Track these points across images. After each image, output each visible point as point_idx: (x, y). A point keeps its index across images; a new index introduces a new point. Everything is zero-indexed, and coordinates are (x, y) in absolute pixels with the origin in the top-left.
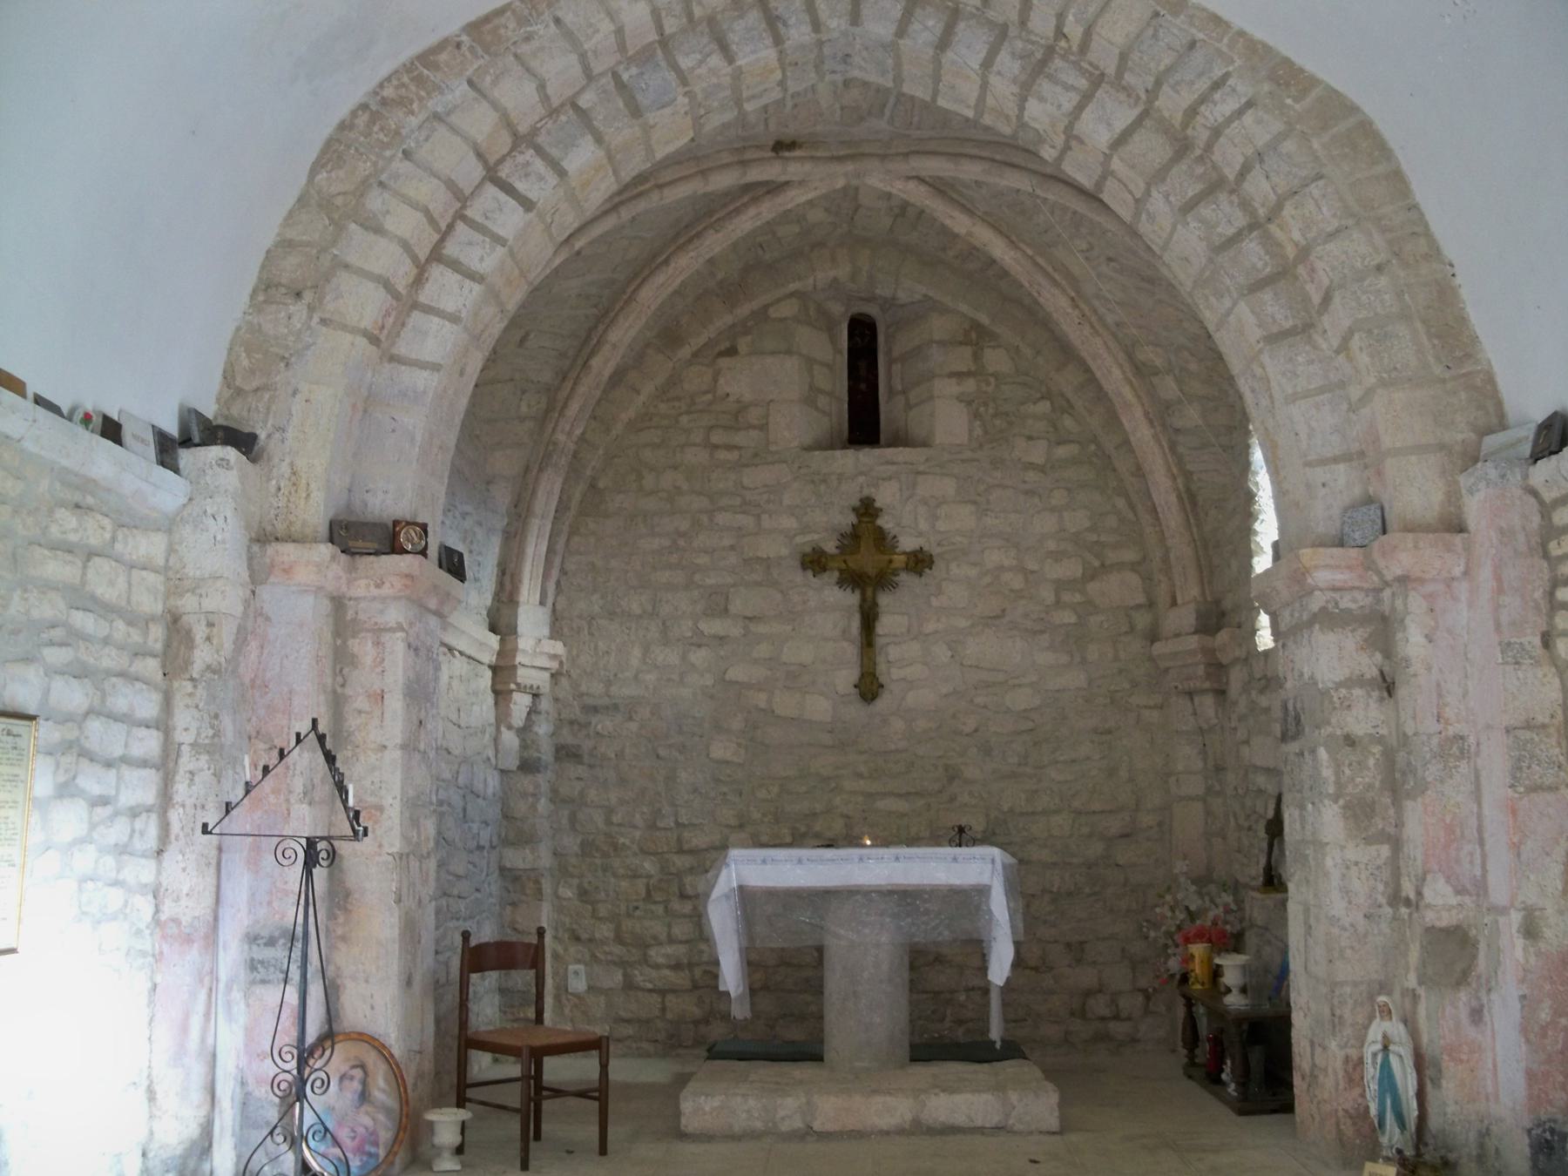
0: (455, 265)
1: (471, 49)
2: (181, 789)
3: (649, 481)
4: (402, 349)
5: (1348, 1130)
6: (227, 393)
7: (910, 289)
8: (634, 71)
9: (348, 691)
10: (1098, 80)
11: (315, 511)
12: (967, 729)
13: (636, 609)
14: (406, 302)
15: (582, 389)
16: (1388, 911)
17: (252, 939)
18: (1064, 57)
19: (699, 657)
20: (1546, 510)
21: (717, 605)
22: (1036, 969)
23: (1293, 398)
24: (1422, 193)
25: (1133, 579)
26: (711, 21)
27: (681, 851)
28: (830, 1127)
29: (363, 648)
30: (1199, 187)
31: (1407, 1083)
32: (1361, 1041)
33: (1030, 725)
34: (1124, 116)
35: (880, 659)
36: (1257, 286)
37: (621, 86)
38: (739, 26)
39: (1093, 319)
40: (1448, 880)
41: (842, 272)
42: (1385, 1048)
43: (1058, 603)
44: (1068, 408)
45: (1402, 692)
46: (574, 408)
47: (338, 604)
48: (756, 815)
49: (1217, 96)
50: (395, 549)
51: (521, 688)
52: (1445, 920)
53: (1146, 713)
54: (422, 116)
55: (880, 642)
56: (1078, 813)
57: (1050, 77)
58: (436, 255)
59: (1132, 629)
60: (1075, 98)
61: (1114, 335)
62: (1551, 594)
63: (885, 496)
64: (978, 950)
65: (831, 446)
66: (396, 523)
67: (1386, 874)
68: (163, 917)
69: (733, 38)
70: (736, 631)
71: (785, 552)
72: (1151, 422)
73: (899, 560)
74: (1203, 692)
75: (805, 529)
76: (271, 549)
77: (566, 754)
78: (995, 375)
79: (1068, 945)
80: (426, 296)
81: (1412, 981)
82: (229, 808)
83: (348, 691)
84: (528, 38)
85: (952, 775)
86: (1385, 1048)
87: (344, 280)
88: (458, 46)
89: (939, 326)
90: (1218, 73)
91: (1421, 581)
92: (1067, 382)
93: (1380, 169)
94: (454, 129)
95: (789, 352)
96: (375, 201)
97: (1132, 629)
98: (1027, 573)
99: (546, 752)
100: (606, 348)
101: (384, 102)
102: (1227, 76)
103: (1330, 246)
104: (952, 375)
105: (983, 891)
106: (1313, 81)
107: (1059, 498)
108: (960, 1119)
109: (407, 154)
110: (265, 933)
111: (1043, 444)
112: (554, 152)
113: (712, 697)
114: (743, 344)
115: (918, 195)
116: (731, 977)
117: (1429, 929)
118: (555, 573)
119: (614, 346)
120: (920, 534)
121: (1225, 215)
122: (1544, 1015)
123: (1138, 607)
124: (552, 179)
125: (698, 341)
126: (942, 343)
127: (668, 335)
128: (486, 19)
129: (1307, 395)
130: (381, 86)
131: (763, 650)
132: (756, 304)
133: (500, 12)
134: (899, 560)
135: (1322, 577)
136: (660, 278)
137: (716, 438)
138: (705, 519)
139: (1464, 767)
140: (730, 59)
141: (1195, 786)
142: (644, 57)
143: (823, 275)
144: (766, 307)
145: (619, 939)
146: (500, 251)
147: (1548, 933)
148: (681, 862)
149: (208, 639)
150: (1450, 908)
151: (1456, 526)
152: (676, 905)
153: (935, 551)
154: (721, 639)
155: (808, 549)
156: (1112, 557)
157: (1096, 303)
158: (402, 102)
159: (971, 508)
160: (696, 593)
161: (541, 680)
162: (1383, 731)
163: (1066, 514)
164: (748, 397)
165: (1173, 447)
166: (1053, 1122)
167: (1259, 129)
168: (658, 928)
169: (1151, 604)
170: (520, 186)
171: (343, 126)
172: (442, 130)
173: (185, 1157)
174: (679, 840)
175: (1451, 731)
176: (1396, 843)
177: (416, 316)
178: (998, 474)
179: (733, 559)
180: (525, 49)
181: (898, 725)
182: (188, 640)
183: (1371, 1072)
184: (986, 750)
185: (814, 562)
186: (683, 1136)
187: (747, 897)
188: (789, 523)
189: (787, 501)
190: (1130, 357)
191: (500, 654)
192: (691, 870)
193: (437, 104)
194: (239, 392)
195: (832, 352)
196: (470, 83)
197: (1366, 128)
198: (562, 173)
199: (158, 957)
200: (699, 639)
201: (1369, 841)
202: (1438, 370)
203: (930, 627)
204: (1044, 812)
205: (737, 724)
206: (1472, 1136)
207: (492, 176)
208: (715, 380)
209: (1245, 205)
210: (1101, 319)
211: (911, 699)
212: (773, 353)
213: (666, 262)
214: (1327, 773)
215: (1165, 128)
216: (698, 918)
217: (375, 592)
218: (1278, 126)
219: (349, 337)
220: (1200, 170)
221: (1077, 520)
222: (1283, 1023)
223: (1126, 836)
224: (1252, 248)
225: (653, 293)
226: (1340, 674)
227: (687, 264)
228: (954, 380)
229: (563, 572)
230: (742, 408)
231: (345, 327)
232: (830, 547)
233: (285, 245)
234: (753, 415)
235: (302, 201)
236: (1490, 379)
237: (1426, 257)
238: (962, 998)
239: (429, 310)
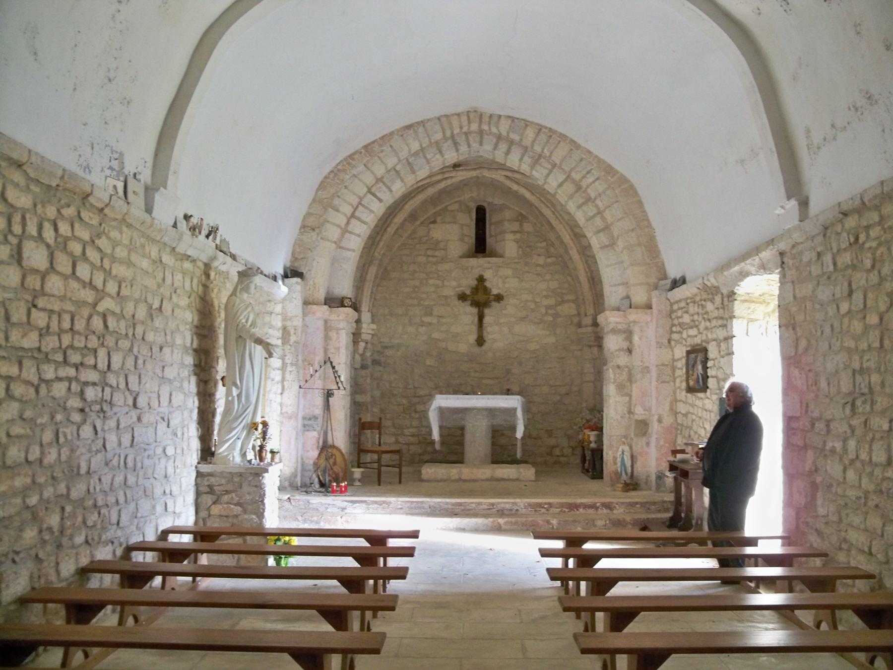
0: (359, 219)
1: (365, 154)
2: (287, 376)
3: (405, 268)
4: (343, 244)
5: (613, 475)
6: (293, 259)
7: (498, 201)
8: (413, 158)
9: (329, 347)
10: (554, 166)
11: (321, 295)
12: (514, 356)
13: (400, 313)
14: (345, 231)
15: (384, 238)
16: (627, 416)
17: (304, 418)
18: (544, 158)
19: (422, 330)
20: (672, 305)
21: (429, 312)
22: (535, 438)
23: (607, 266)
24: (647, 207)
25: (573, 306)
26: (437, 142)
27: (415, 396)
28: (467, 478)
29: (333, 334)
30: (583, 200)
31: (628, 463)
32: (617, 450)
33: (535, 355)
34: (562, 177)
35: (485, 332)
36: (598, 232)
37: (409, 163)
38: (445, 145)
39: (560, 218)
40: (642, 407)
41: (474, 194)
42: (623, 453)
43: (546, 313)
44: (553, 245)
45: (633, 353)
46: (381, 244)
47: (326, 322)
48: (441, 384)
49: (588, 176)
50: (343, 306)
51: (362, 341)
52: (640, 418)
53: (576, 352)
54: (350, 175)
55: (485, 325)
56: (551, 386)
57: (540, 165)
58: (353, 216)
59: (572, 323)
60: (547, 171)
61: (567, 224)
62: (671, 328)
63: (488, 275)
64: (513, 428)
65: (469, 257)
66: (343, 298)
67: (627, 405)
68: (283, 411)
69: (443, 149)
70: (435, 321)
71: (452, 294)
72: (579, 254)
73: (492, 298)
74: (594, 346)
75: (459, 286)
76: (310, 307)
77: (375, 362)
78: (528, 233)
79: (547, 431)
80: (350, 228)
81: (632, 436)
82: (306, 381)
83: (329, 347)
84: (382, 151)
85: (508, 372)
86: (623, 453)
87: (327, 225)
88: (361, 153)
89: (508, 214)
90: (589, 168)
91: (639, 322)
92: (552, 236)
93: (635, 199)
94: (360, 179)
95: (455, 223)
96: (336, 201)
97: (572, 323)
98: (536, 302)
99: (369, 362)
100: (393, 225)
101: (339, 170)
102: (592, 169)
103: (618, 223)
104: (512, 232)
105: (515, 409)
106: (617, 172)
107: (548, 277)
108: (506, 476)
109: (346, 187)
110: (308, 417)
111: (543, 257)
112: (389, 184)
113: (427, 343)
114: (439, 219)
115: (502, 179)
116: (436, 435)
117: (636, 421)
118: (373, 300)
119: (396, 224)
120: (499, 288)
121: (590, 210)
122: (662, 443)
123: (574, 315)
124: (388, 193)
125: (422, 219)
126: (509, 221)
127: (413, 217)
128: (369, 144)
129: (611, 265)
130: (337, 165)
131: (444, 328)
132: (443, 206)
133: (373, 142)
134: (492, 298)
135: (612, 319)
136: (411, 202)
137: (429, 253)
138: (425, 281)
139: (648, 375)
140: (442, 156)
141: (590, 377)
142: (416, 154)
143: (467, 196)
144: (447, 206)
145: (394, 426)
146: (373, 215)
147: (664, 421)
148: (416, 400)
149: (295, 334)
150: (641, 414)
151: (649, 307)
152: (413, 415)
153: (504, 294)
154: (430, 324)
155: (460, 293)
156: (566, 298)
157: (561, 213)
158: (344, 171)
159: (517, 280)
160: (421, 308)
161: (368, 337)
162: (628, 364)
163: (550, 282)
164: (440, 239)
165: (587, 262)
166: (533, 478)
167: (600, 187)
168: (407, 423)
169: (579, 314)
170: (378, 194)
171: (326, 178)
172: (356, 180)
173: (290, 477)
174: (415, 393)
175: (645, 365)
176: (630, 396)
177: (347, 235)
178: (527, 268)
179: (434, 296)
180: (381, 155)
181: (490, 354)
182: (289, 334)
183: (619, 460)
184: (520, 363)
185: (462, 297)
186: (423, 481)
187: (442, 411)
188: (454, 284)
189: (453, 275)
190: (573, 231)
191: (356, 329)
192: (419, 403)
193: (354, 172)
194: (296, 259)
195: (469, 221)
196: (365, 165)
197: (632, 187)
198: (391, 191)
199: (282, 423)
200: (422, 324)
201: (622, 396)
202: (648, 261)
203: (502, 321)
204: (539, 385)
205: (435, 353)
206: (644, 477)
207: (370, 191)
208: (429, 232)
209: (597, 206)
210: (563, 218)
211: (495, 345)
212: (449, 223)
213: (414, 196)
214: (612, 376)
215: (574, 182)
216: (427, 418)
217: (337, 318)
218: (606, 186)
219: (330, 243)
220: (584, 195)
221: (554, 285)
222: (602, 451)
223: (567, 394)
224: (598, 220)
225: (409, 207)
226: (617, 348)
227: (422, 197)
228: (512, 234)
229: (375, 299)
230: (438, 242)
231: (328, 240)
232: (468, 292)
233: (308, 214)
234: (442, 245)
235: (314, 200)
236: (663, 264)
237: (647, 227)
238: (510, 448)
239: (351, 233)
